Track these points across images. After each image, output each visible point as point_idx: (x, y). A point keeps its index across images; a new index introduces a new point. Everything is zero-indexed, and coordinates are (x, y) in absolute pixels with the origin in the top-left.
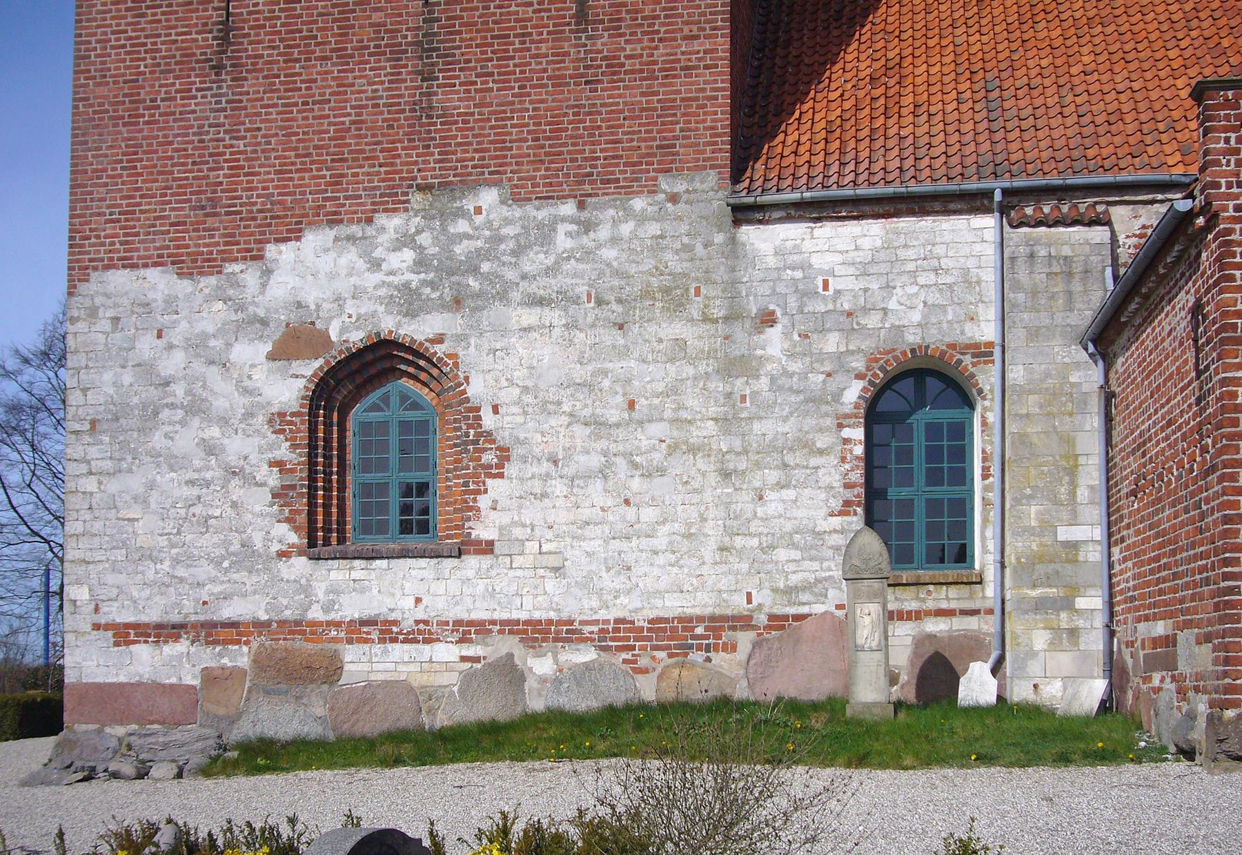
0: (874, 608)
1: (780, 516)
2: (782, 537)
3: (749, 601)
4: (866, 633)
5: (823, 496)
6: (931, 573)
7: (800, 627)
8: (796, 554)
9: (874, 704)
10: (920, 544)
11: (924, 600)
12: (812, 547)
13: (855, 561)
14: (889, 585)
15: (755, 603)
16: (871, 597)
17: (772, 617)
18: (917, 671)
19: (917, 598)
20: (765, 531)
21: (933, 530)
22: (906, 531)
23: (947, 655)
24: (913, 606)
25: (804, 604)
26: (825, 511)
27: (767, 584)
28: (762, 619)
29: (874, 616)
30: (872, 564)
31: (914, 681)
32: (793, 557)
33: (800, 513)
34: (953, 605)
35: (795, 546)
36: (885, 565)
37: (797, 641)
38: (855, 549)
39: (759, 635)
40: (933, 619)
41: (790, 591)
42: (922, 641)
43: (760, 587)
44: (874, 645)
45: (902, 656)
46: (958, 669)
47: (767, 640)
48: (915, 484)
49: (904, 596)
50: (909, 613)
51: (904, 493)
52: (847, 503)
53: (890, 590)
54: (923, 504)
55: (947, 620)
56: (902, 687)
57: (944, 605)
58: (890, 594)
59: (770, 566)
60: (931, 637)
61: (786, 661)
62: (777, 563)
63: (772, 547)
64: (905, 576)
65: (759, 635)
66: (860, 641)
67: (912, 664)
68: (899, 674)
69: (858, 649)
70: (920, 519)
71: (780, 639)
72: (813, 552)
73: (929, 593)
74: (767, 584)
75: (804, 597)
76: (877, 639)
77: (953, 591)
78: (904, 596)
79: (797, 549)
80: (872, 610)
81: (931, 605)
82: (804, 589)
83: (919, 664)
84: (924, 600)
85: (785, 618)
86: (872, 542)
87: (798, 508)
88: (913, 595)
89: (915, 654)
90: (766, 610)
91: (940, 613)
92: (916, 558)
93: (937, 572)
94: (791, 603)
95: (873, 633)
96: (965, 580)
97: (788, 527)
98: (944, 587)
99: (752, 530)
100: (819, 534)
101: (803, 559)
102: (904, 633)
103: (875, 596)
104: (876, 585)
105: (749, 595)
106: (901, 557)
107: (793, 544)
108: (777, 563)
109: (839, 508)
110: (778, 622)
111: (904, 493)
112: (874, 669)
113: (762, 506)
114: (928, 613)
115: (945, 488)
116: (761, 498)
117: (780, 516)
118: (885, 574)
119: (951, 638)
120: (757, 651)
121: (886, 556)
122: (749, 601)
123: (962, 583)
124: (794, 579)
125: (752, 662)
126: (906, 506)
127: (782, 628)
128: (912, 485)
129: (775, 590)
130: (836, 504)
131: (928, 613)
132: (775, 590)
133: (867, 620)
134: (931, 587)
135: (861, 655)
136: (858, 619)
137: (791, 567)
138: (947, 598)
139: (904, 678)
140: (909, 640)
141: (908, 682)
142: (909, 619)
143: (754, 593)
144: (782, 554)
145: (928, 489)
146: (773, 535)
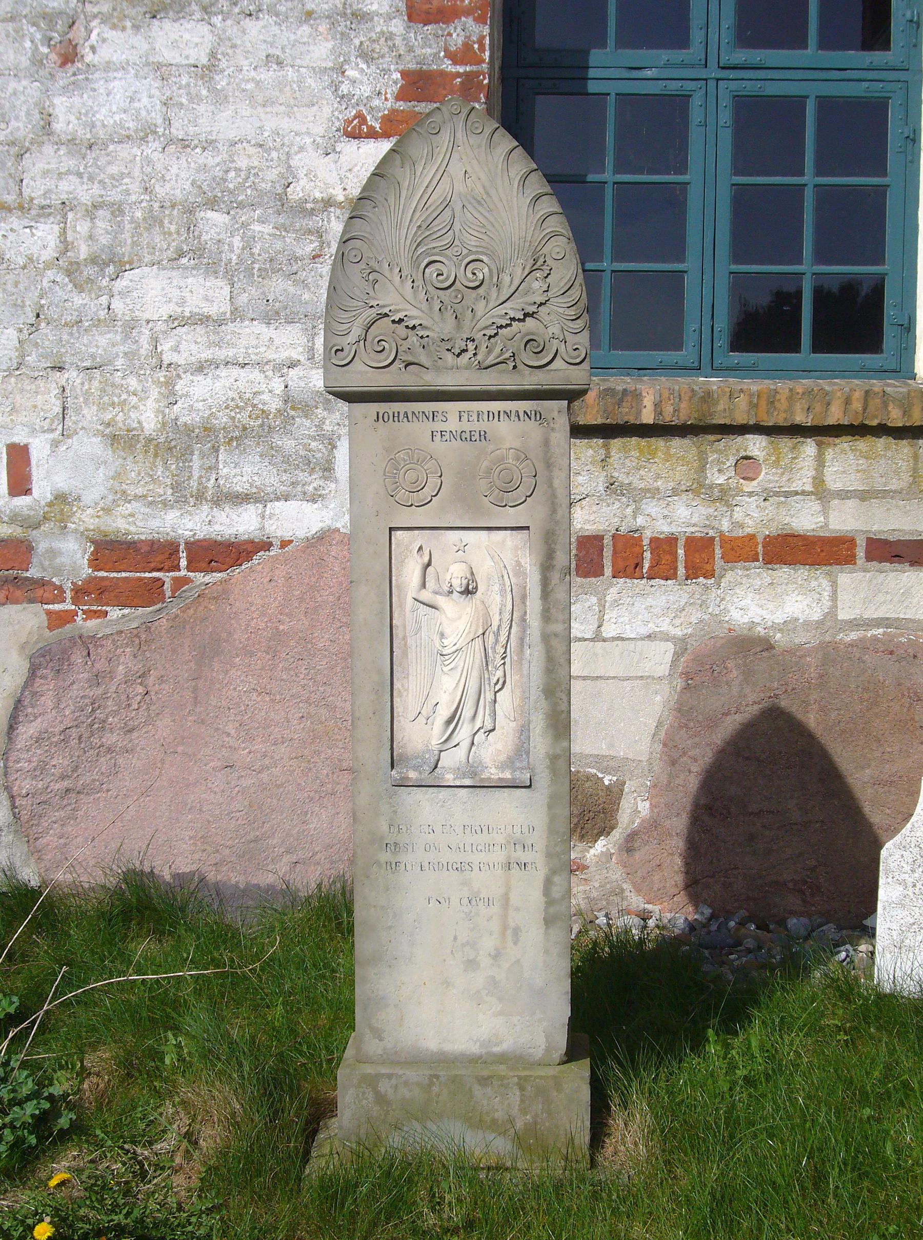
0: (499, 558)
1: (146, 133)
2: (153, 221)
3: (20, 484)
4: (447, 690)
5: (322, 51)
6: (754, 386)
7: (221, 594)
8: (207, 293)
9: (488, 1068)
10: (709, 278)
11: (724, 497)
12: (272, 266)
13: (398, 297)
14: (579, 431)
15: (42, 488)
16: (491, 495)
17: (109, 550)
18: (693, 783)
19: (698, 488)
20: (85, 194)
21: (760, 221)
22: (654, 218)
23: (811, 720)
24: (680, 517)
25: (240, 499)
26: (324, 117)
27: (90, 413)
28: (67, 556)
29: (494, 598)
30: (488, 312)
31: (679, 823)
32: (195, 304)
33: (229, 123)
34: (844, 519)
35: (197, 256)
36: (561, 324)
37: (210, 650)
38: (395, 231)
39: (65, 618)
40: (759, 575)
41: (181, 444)
42: (709, 662)
43: (63, 423)
44: (493, 752)
45: (629, 719)
46: (876, 817)
47: (88, 643)
48: (697, 36)
49: (642, 479)
50: (664, 546)
51: (653, 69)
52: (418, 84)
53: (587, 451)
54: (726, 116)
55: (818, 580)
56: (629, 845)
57: (806, 519)
58: (586, 467)
59: (101, 342)
60: (751, 647)
61: (164, 727)
62: (131, 326)
63: (113, 262)
64: (650, 399)
65: (58, 620)
66: (419, 734)
67: (672, 751)
68: (615, 794)
69: (403, 771)
70: (709, 174)
71: (141, 639)
72: (278, 286)
73: (746, 465)
74: (90, 413)
75: (242, 470)
76: (507, 727)
77: (844, 464)
78: (642, 479)
79: (212, 269)
80: (485, 568)
81: (751, 516)
82: (239, 437)
83: (701, 756)
84: (724, 497)
85: (163, 553)
86: (489, 194)
87: (220, 99)
88: (682, 474)
89: (686, 714)
90: (87, 519)
91: (790, 550)
92: (691, 327)
93: (782, 386)
94: (184, 496)
95: (488, 687)
96: (896, 418)
97: (179, 177)
98: (809, 448)
99: (35, 188)
100: (302, 210)
101: (237, 314)
102: (635, 634)
103: (506, 491)
104: (510, 430)
105: (19, 457)
106: (633, 313)
107: (199, 252)
108: (131, 326)
109: (386, 104)
110: (132, 569)
111: (653, 69)
112: (488, 882)
113: (73, 87)
114: (742, 550)
115: (811, 54)
116: (69, 55)
117: (146, 133)
118: (562, 374)
119: (830, 653)
120: (47, 687)
121: (566, 271)
122: (20, 484)
123: (883, 430)
124: (202, 395)
125: (27, 731)
126: (659, 124)
127: (151, 593)
128: (683, 42)
129: (122, 440)
130: (374, 89)
131: (742, 550)
132: (122, 440)
133: (456, 621)
134: (756, 445)
135: (423, 807)
136: (407, 614)
137: (189, 346)
138: (820, 492)
139: (635, 808)
140: (659, 659)
141: (653, 825)
142: (663, 570)
143: (39, 449)
144: (153, 292)
145: (742, 56)
146: (117, 210)
